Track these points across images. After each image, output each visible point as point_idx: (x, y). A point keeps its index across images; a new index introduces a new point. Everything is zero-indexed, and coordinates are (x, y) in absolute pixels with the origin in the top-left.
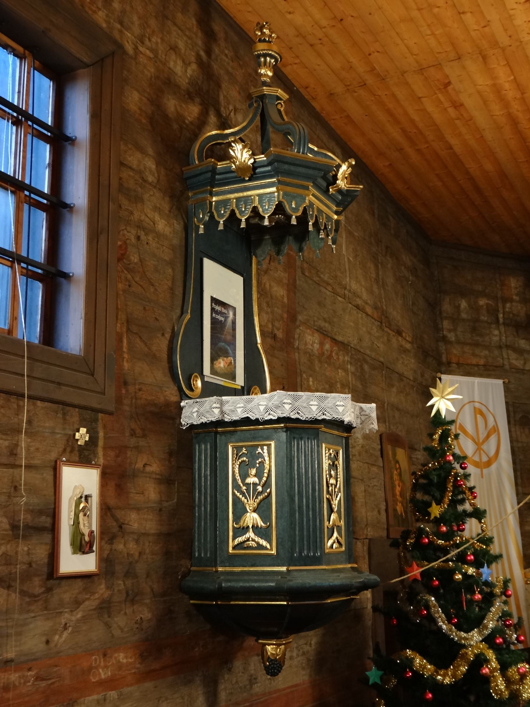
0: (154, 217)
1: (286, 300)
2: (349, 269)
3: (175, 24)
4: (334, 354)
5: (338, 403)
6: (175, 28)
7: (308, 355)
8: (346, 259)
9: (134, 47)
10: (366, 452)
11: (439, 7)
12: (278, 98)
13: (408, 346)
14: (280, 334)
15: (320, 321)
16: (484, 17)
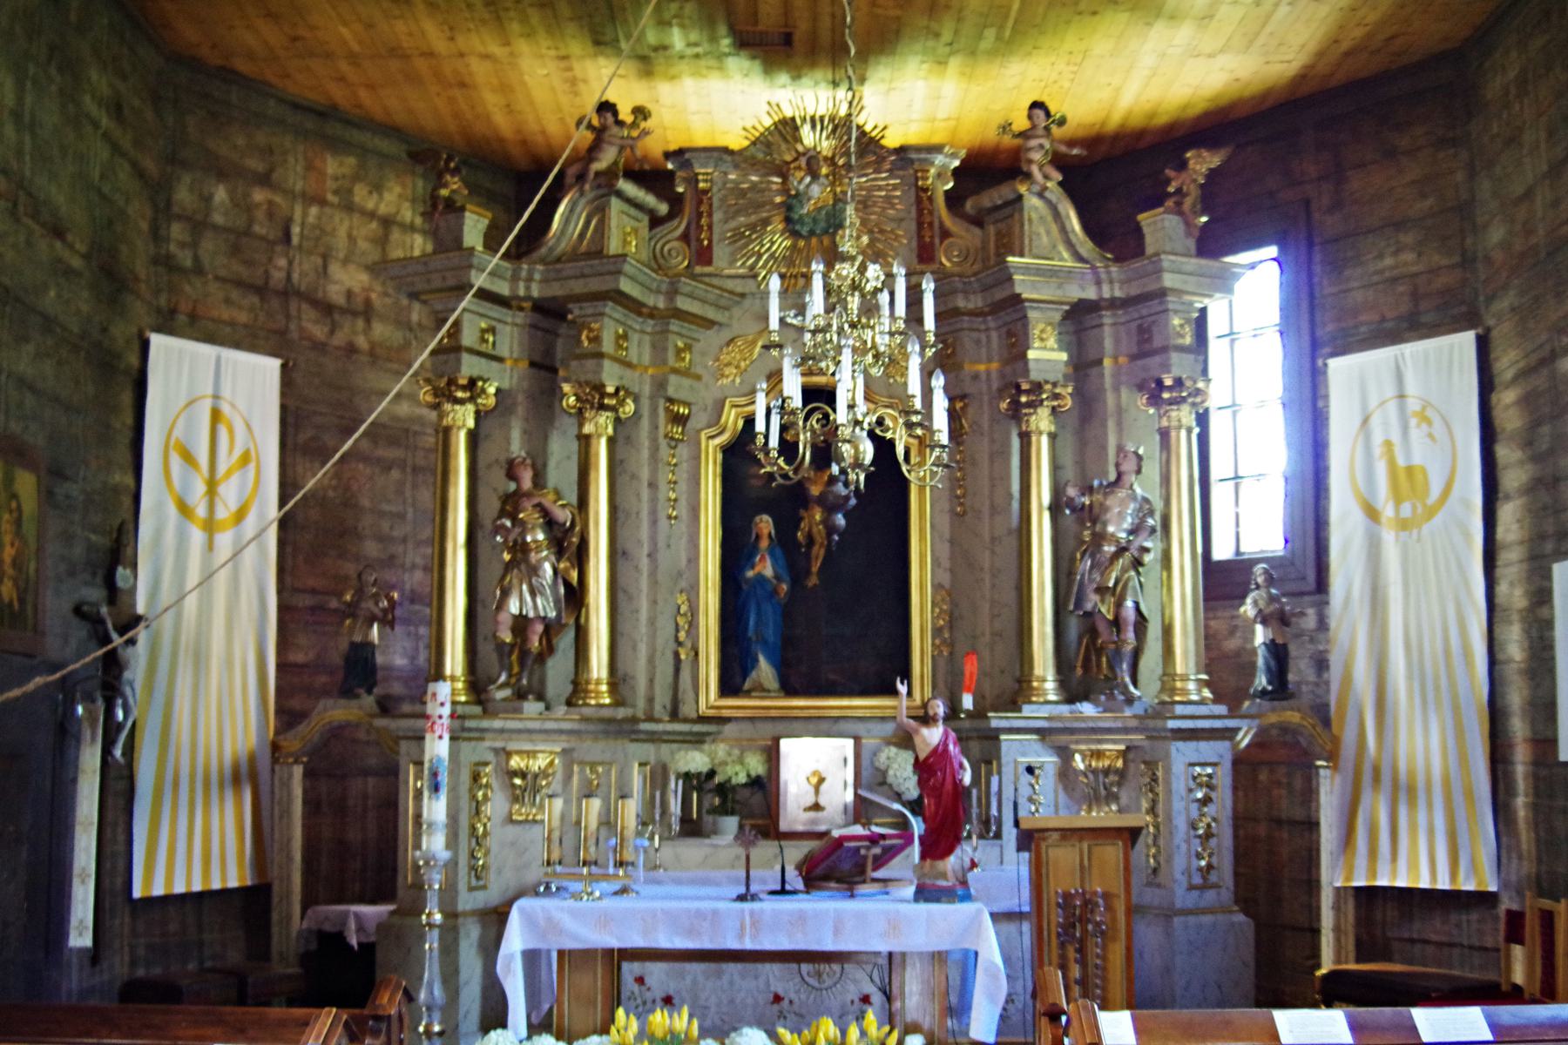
13: (76, 263)
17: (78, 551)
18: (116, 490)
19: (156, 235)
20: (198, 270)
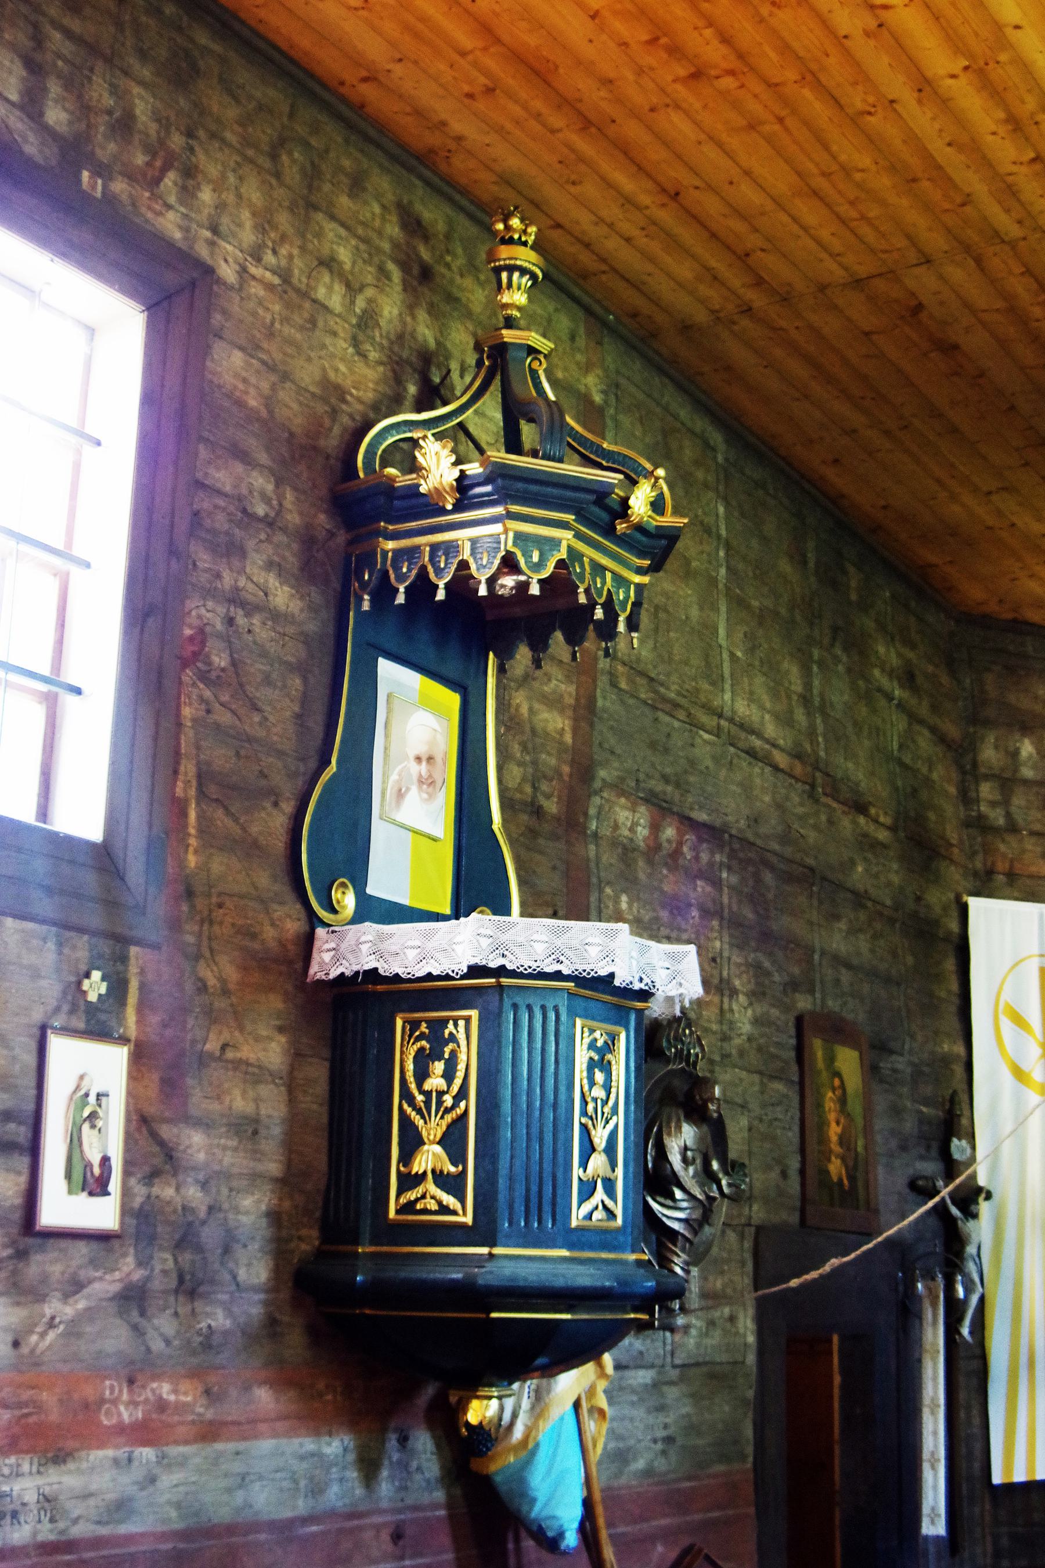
0: (267, 581)
1: (568, 738)
2: (732, 675)
3: (333, 217)
4: (685, 849)
5: (535, 937)
6: (333, 225)
7: (620, 850)
8: (725, 656)
9: (237, 268)
10: (760, 1049)
11: (862, 171)
12: (532, 351)
13: (883, 835)
14: (552, 807)
15: (653, 782)
16: (955, 187)
17: (909, 1125)
18: (946, 1061)
19: (967, 798)
20: (1013, 828)
